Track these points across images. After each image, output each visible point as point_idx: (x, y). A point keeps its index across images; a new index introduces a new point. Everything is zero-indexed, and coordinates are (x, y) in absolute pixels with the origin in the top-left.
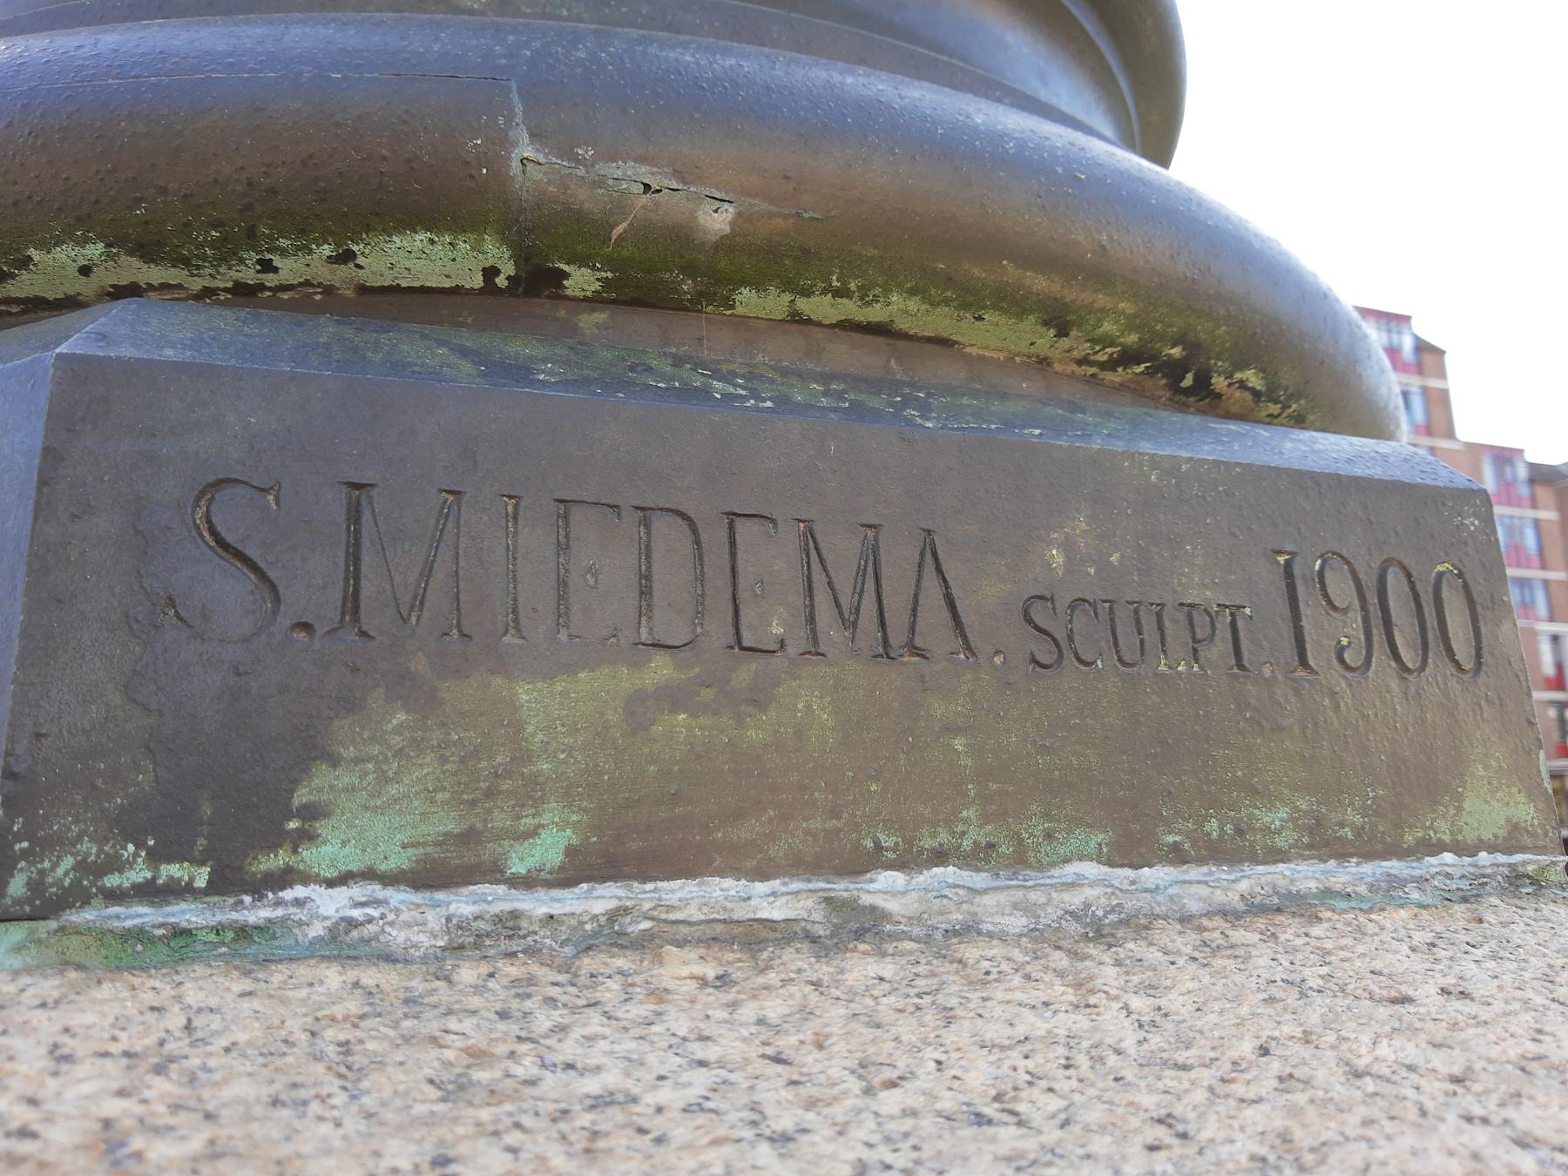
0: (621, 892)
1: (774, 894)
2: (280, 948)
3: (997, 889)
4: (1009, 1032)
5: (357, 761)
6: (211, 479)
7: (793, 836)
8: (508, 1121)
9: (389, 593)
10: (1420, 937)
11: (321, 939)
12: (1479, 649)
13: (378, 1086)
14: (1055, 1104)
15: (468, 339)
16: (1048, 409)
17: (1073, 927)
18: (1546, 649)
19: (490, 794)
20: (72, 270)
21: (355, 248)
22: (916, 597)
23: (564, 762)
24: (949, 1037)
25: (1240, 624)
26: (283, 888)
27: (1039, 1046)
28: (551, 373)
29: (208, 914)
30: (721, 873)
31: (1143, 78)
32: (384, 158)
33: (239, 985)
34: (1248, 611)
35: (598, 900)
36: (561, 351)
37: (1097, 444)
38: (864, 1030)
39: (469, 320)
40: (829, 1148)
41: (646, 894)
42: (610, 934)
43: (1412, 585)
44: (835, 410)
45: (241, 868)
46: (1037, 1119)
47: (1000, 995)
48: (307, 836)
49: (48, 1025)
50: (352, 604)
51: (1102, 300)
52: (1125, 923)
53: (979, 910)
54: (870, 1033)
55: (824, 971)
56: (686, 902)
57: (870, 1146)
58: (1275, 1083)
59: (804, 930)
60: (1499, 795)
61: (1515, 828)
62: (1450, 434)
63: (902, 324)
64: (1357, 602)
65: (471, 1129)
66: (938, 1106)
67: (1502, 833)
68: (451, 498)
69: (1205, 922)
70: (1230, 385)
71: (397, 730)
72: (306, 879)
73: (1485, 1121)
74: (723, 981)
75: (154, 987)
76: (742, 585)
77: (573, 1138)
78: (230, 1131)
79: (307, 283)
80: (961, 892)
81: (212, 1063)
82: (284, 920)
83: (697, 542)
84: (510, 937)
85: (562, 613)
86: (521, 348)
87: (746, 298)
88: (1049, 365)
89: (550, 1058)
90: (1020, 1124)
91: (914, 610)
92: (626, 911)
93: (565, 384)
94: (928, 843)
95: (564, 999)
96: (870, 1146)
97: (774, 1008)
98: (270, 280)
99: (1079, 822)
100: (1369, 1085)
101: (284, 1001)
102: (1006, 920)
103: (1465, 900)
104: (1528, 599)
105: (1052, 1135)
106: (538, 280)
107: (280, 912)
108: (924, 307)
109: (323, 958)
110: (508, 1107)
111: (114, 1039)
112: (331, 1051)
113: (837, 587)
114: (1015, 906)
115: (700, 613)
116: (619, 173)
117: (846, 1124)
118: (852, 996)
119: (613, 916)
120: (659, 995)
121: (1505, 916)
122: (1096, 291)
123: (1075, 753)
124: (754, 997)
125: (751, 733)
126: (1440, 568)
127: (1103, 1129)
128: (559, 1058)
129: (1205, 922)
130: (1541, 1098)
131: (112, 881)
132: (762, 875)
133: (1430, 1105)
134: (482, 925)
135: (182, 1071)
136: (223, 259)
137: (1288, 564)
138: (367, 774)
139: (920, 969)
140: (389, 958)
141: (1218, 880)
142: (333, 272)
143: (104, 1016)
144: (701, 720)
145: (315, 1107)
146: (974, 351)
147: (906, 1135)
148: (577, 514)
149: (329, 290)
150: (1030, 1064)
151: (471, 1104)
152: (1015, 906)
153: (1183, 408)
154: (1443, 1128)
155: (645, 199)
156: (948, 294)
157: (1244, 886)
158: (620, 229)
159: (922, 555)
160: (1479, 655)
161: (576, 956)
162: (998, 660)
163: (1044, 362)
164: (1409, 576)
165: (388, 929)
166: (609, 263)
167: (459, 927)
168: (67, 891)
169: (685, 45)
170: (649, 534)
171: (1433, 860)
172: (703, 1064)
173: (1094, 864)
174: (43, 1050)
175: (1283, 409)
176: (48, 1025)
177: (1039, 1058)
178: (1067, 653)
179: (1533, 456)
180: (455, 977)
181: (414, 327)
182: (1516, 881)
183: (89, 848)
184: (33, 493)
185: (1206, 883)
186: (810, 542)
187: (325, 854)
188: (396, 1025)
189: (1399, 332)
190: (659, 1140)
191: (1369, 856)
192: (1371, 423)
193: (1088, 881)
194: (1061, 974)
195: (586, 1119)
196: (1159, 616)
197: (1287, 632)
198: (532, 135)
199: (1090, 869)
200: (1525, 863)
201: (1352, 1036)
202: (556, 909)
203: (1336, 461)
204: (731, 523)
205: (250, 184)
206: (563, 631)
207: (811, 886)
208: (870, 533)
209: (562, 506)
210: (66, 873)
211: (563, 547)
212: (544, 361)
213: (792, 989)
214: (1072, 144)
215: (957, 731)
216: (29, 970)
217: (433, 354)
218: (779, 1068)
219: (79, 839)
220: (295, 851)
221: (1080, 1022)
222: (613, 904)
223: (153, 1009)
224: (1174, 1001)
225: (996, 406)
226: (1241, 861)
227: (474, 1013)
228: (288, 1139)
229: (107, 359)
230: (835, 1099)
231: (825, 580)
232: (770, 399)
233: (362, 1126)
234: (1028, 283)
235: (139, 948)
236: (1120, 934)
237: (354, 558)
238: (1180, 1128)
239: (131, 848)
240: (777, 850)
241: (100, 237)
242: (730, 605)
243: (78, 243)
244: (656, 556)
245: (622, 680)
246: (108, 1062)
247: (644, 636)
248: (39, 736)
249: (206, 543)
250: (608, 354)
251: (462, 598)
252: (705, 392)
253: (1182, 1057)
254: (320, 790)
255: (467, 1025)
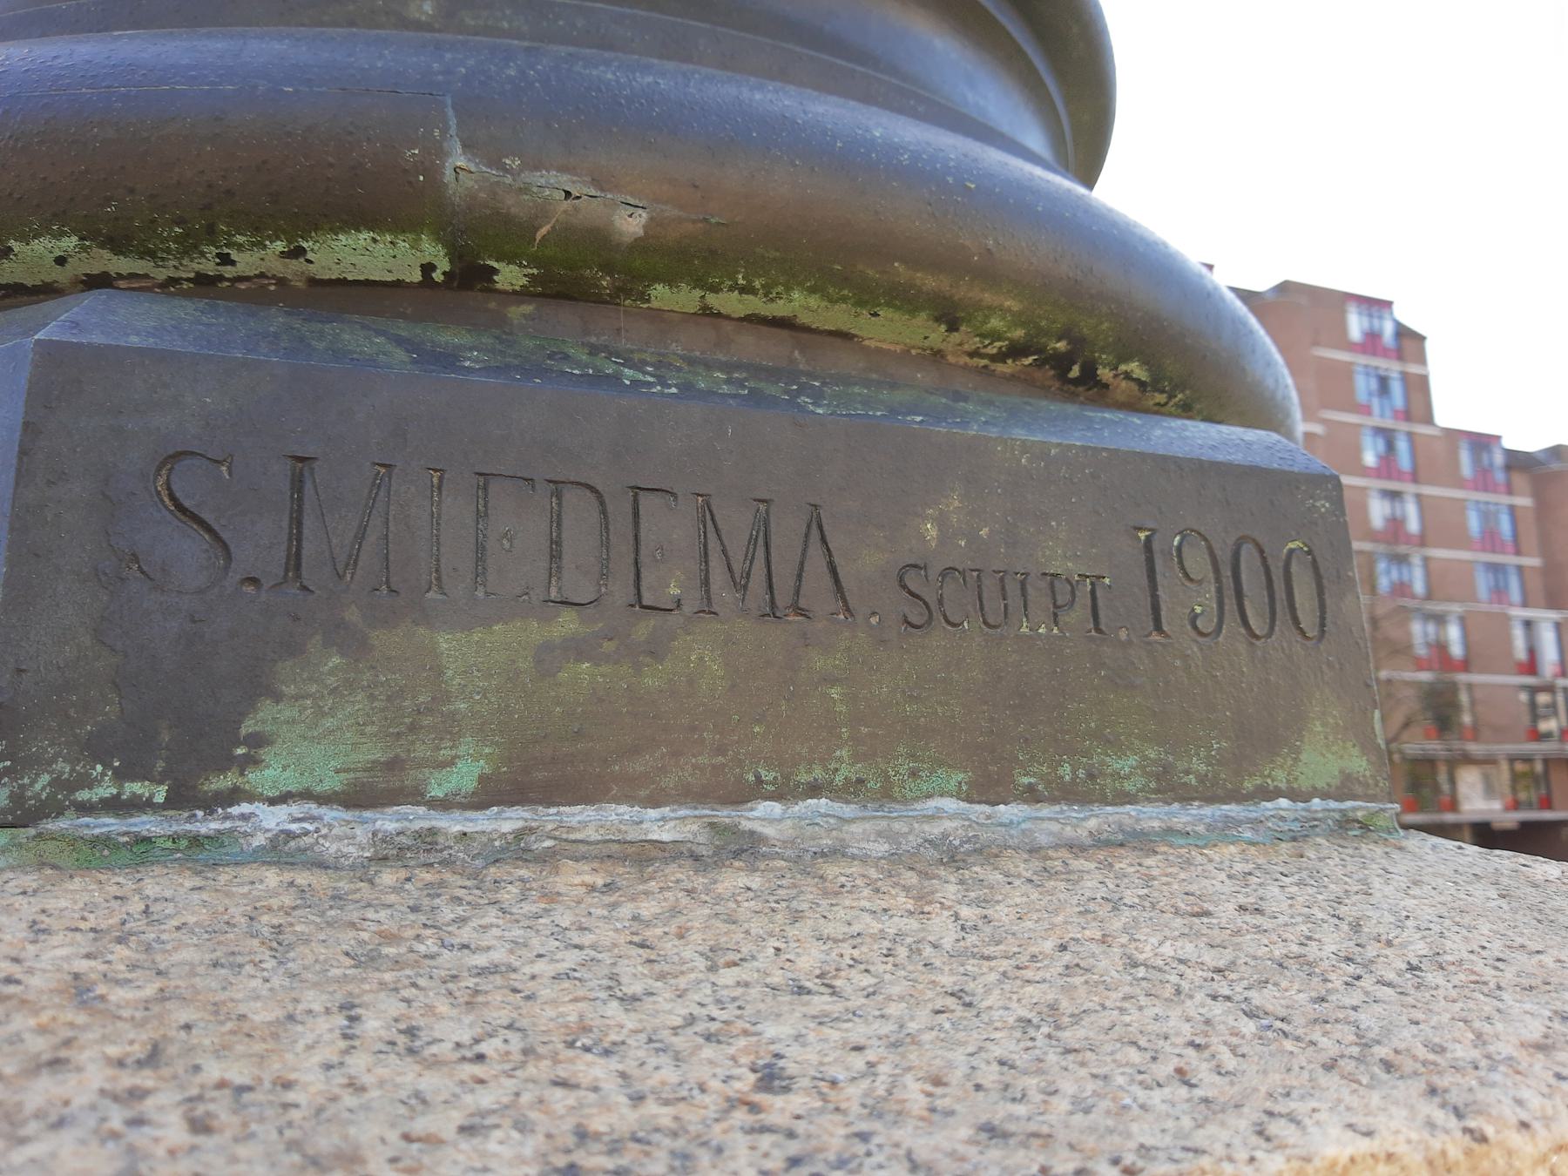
0: (527, 815)
1: (663, 819)
2: (227, 854)
3: (863, 819)
4: (846, 929)
5: (297, 698)
6: (171, 452)
7: (683, 769)
8: (407, 982)
9: (327, 554)
10: (1239, 867)
11: (263, 848)
12: (1323, 618)
13: (301, 957)
14: (867, 981)
15: (403, 329)
16: (932, 398)
17: (932, 853)
18: (1518, 634)
19: (413, 728)
20: (50, 259)
21: (305, 245)
22: (802, 564)
23: (479, 702)
24: (792, 932)
25: (1099, 594)
26: (231, 805)
27: (868, 940)
28: (476, 361)
29: (166, 825)
30: (617, 800)
31: (1074, 88)
32: (331, 165)
33: (190, 882)
34: (1107, 581)
35: (509, 820)
36: (487, 340)
37: (974, 430)
38: (721, 925)
39: (409, 311)
40: (668, 1006)
41: (548, 817)
42: (518, 849)
43: (1264, 560)
44: (735, 396)
45: (194, 787)
46: (848, 990)
47: (847, 903)
48: (252, 761)
49: (28, 908)
50: (295, 562)
51: (987, 297)
52: (979, 851)
53: (847, 837)
54: (724, 927)
55: (700, 881)
56: (584, 825)
57: (702, 1005)
58: (1060, 970)
59: (690, 850)
60: (1335, 748)
61: (1347, 778)
62: (1428, 419)
63: (804, 319)
64: (1211, 575)
65: (375, 986)
66: (768, 980)
67: (1336, 782)
68: (383, 470)
69: (1050, 853)
70: (1116, 376)
71: (331, 672)
72: (251, 798)
73: (1228, 998)
74: (609, 887)
75: (120, 881)
76: (643, 551)
77: (458, 994)
78: (176, 982)
79: (262, 275)
80: (832, 821)
81: (164, 937)
82: (231, 831)
83: (604, 512)
84: (429, 851)
85: (480, 572)
86: (450, 337)
87: (660, 294)
88: (943, 357)
89: (448, 940)
90: (833, 994)
91: (799, 577)
92: (531, 830)
93: (487, 370)
94: (804, 778)
95: (469, 898)
96: (702, 1005)
97: (648, 909)
98: (228, 272)
99: (941, 764)
100: (1141, 972)
101: (228, 894)
102: (871, 846)
103: (1294, 839)
104: (1502, 584)
105: (858, 1001)
106: (471, 275)
107: (228, 825)
108: (824, 304)
109: (264, 863)
110: (408, 972)
111: (84, 919)
112: (266, 931)
113: (730, 554)
114: (879, 834)
115: (604, 574)
116: (542, 181)
117: (686, 990)
118: (719, 899)
119: (519, 835)
120: (552, 897)
121: (1325, 852)
122: (983, 290)
123: (940, 703)
124: (633, 900)
125: (648, 681)
126: (1292, 545)
127: (902, 998)
128: (456, 941)
129: (1050, 853)
130: (1284, 984)
131: (83, 795)
132: (655, 803)
133: (1185, 985)
134: (403, 839)
135: (139, 942)
136: (186, 252)
137: (1148, 538)
138: (305, 709)
139: (784, 882)
140: (322, 865)
141: (1068, 818)
142: (286, 266)
143: (75, 902)
144: (604, 669)
145: (249, 969)
146: (873, 344)
147: (734, 999)
148: (494, 487)
149: (281, 282)
150: (856, 953)
151: (378, 970)
152: (879, 834)
153: (1072, 397)
154: (1189, 1003)
155: (567, 205)
156: (845, 292)
157: (1092, 823)
158: (543, 231)
159: (809, 527)
160: (1322, 625)
161: (484, 868)
162: (874, 620)
163: (938, 355)
164: (1261, 552)
165: (321, 841)
166: (534, 261)
167: (384, 841)
168: (43, 804)
169: (607, 63)
170: (560, 504)
171: (1268, 805)
172: (579, 947)
173: (954, 800)
174: (24, 925)
175: (1171, 397)
176: (28, 908)
177: (864, 949)
178: (937, 615)
179: (1509, 443)
180: (377, 880)
181: (356, 317)
182: (1345, 823)
183: (62, 767)
184: (15, 461)
185: (1057, 820)
186: (707, 514)
187: (268, 777)
188: (322, 914)
189: (1381, 318)
190: (528, 998)
191: (1210, 800)
192: (1260, 411)
193: (948, 813)
194: (906, 889)
195: (471, 982)
196: (1023, 584)
197: (1147, 602)
198: (465, 146)
199: (950, 804)
200: (1355, 809)
201: (1143, 938)
202: (469, 828)
203: (1201, 447)
204: (636, 496)
205: (210, 186)
206: (481, 588)
207: (697, 813)
208: (762, 507)
209: (482, 479)
210: (43, 788)
211: (481, 516)
212: (471, 349)
213: (668, 894)
214: (965, 156)
215: (834, 682)
216: (12, 868)
217: (372, 343)
218: (641, 951)
219: (53, 760)
220: (242, 774)
221: (913, 924)
222: (520, 824)
223: (116, 898)
224: (1001, 913)
225: (885, 394)
226: (1091, 802)
227: (390, 906)
228: (224, 989)
229: (80, 346)
230: (682, 973)
231: (719, 548)
232: (676, 386)
233: (287, 982)
234: (918, 282)
235: (106, 852)
236: (971, 860)
237: (297, 521)
238: (967, 999)
239: (99, 768)
240: (669, 781)
241: (74, 231)
242: (632, 569)
243: (54, 237)
244: (566, 523)
245: (535, 632)
246: (78, 936)
247: (553, 594)
248: (20, 671)
249: (166, 507)
250: (531, 344)
251: (391, 558)
252: (616, 379)
253: (990, 950)
254: (264, 722)
255: (383, 915)
